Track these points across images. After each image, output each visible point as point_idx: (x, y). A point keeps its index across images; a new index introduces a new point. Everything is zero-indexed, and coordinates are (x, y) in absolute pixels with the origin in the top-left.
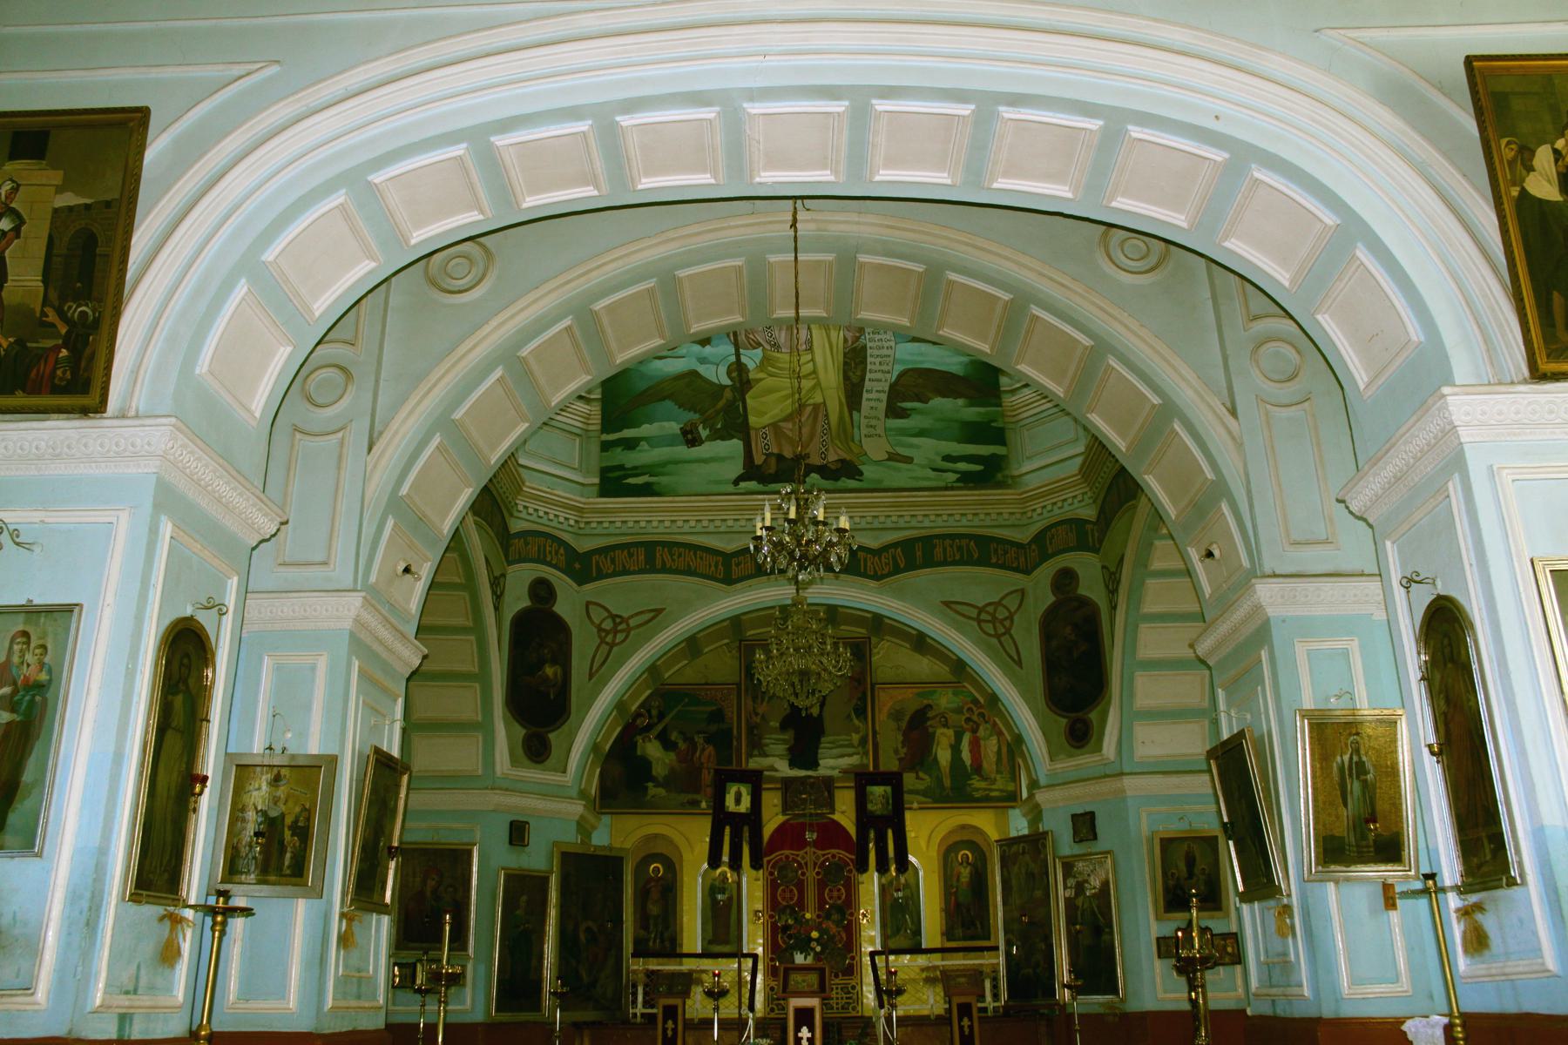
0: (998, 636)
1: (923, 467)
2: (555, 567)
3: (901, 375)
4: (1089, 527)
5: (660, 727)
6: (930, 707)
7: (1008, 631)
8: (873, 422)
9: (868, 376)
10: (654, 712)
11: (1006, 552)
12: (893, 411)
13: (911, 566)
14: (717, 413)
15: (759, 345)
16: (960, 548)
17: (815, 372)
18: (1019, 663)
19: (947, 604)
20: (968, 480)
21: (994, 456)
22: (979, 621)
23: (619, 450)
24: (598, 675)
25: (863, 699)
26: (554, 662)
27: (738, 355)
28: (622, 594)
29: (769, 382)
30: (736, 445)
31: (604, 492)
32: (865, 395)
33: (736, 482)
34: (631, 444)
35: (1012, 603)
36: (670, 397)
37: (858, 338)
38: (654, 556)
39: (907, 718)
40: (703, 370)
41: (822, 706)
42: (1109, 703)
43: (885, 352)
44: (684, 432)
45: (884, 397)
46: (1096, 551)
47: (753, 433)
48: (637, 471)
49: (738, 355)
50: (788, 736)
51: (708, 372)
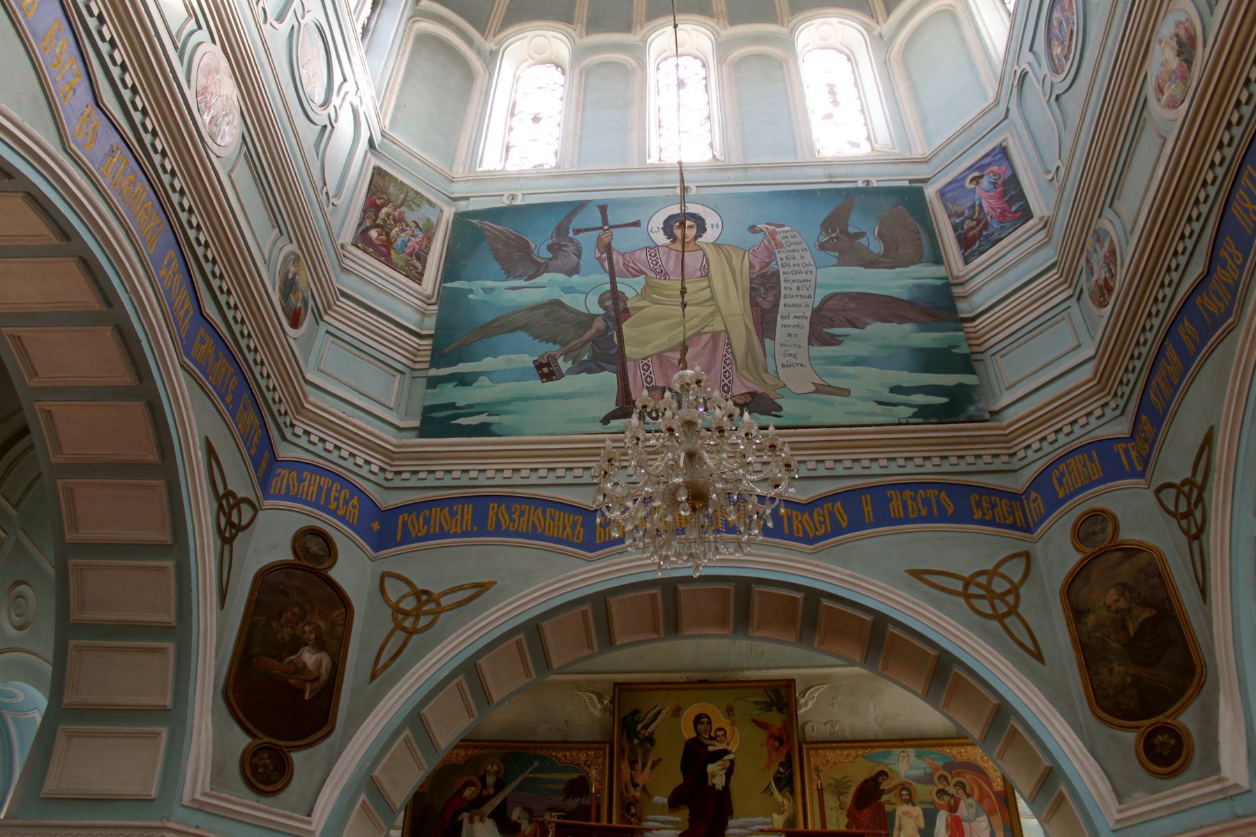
0: (1000, 618)
1: (865, 400)
2: (342, 519)
3: (825, 300)
4: (1119, 447)
5: (497, 801)
6: (883, 773)
7: (1013, 610)
8: (793, 350)
9: (782, 301)
10: (490, 780)
11: (994, 506)
12: (818, 337)
13: (857, 524)
14: (584, 344)
15: (642, 272)
16: (926, 502)
17: (712, 298)
18: (1038, 656)
19: (917, 574)
20: (925, 413)
21: (960, 385)
22: (968, 597)
23: (451, 386)
24: (382, 671)
25: (788, 764)
26: (319, 645)
27: (613, 283)
28: (433, 566)
29: (653, 310)
30: (609, 378)
31: (423, 431)
32: (780, 322)
33: (605, 421)
34: (464, 380)
35: (1015, 571)
36: (524, 327)
37: (768, 264)
38: (483, 513)
39: (852, 790)
40: (566, 299)
41: (729, 773)
42: (1215, 693)
43: (803, 276)
44: (539, 366)
45: (806, 323)
46: (1142, 475)
47: (630, 365)
48: (471, 410)
49: (613, 283)
50: (681, 817)
51: (575, 302)
